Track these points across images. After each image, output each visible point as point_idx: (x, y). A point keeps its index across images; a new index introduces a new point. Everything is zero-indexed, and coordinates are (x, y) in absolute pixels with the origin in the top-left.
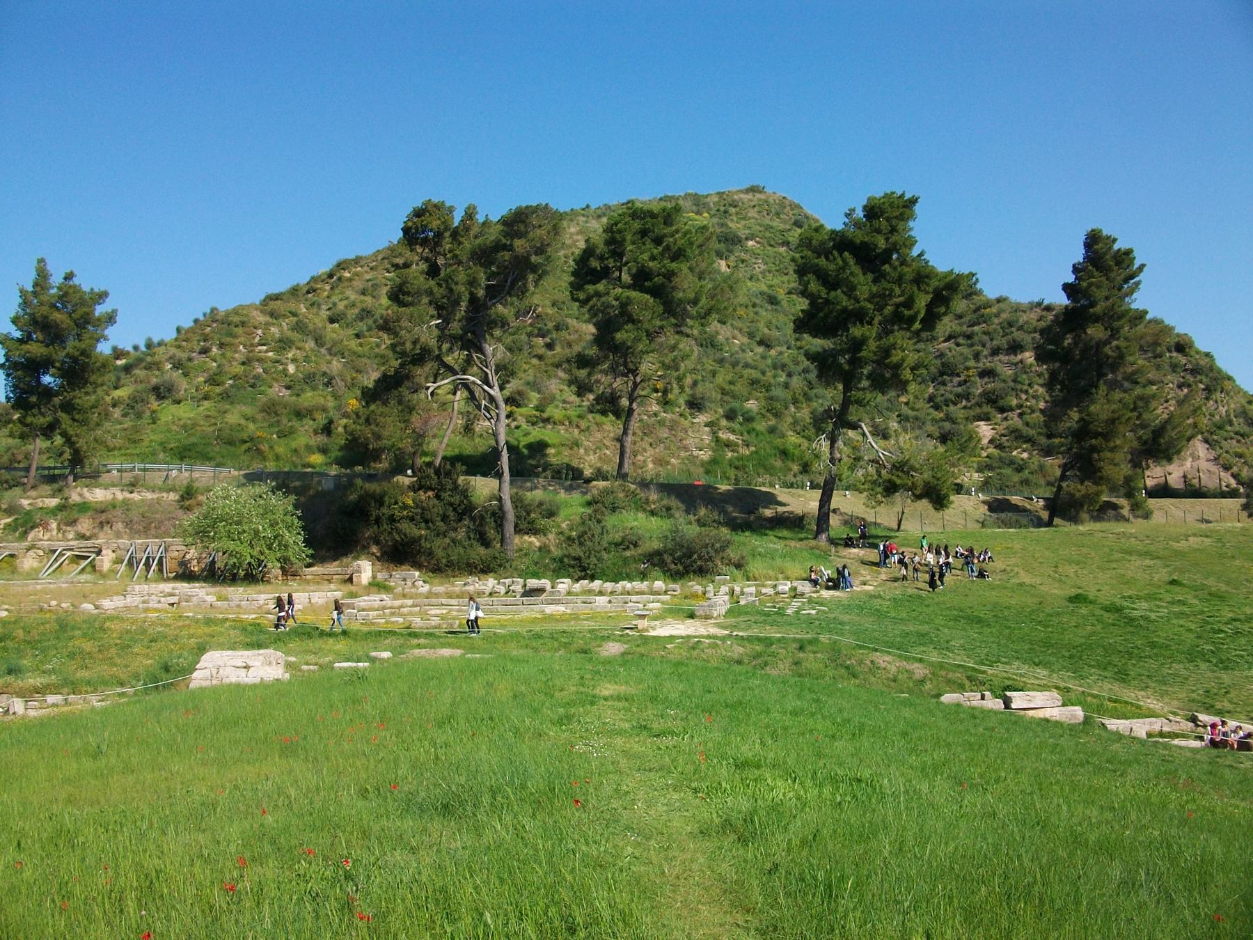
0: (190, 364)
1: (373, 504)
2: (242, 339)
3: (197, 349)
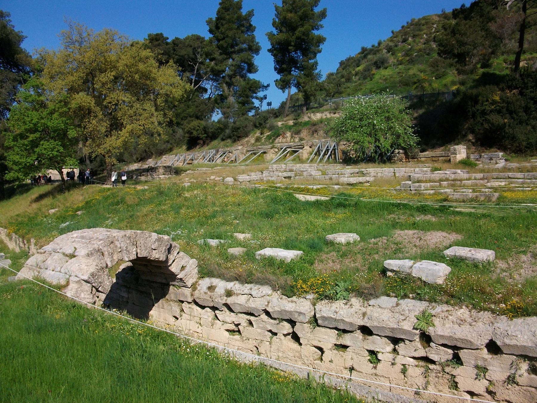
0: (396, 48)
1: (470, 103)
2: (425, 31)
3: (401, 40)
